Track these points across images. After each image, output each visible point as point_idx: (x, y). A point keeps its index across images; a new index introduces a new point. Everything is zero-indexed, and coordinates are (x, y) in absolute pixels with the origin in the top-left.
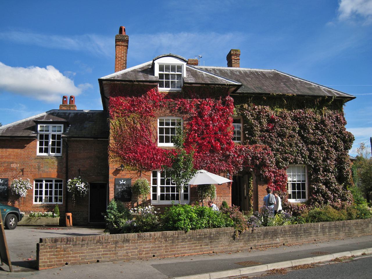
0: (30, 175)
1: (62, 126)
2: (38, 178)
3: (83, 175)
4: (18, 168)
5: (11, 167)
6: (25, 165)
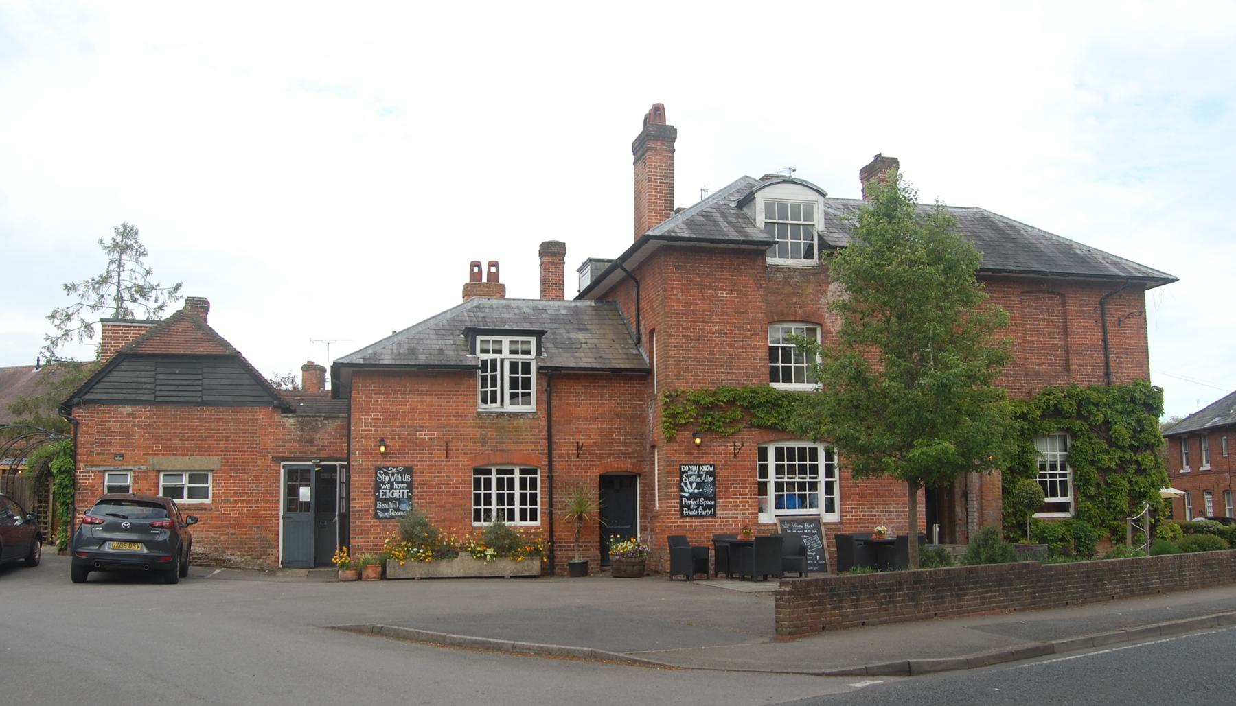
0: (462, 457)
1: (533, 340)
2: (479, 464)
3: (587, 458)
4: (433, 442)
5: (417, 439)
6: (450, 435)
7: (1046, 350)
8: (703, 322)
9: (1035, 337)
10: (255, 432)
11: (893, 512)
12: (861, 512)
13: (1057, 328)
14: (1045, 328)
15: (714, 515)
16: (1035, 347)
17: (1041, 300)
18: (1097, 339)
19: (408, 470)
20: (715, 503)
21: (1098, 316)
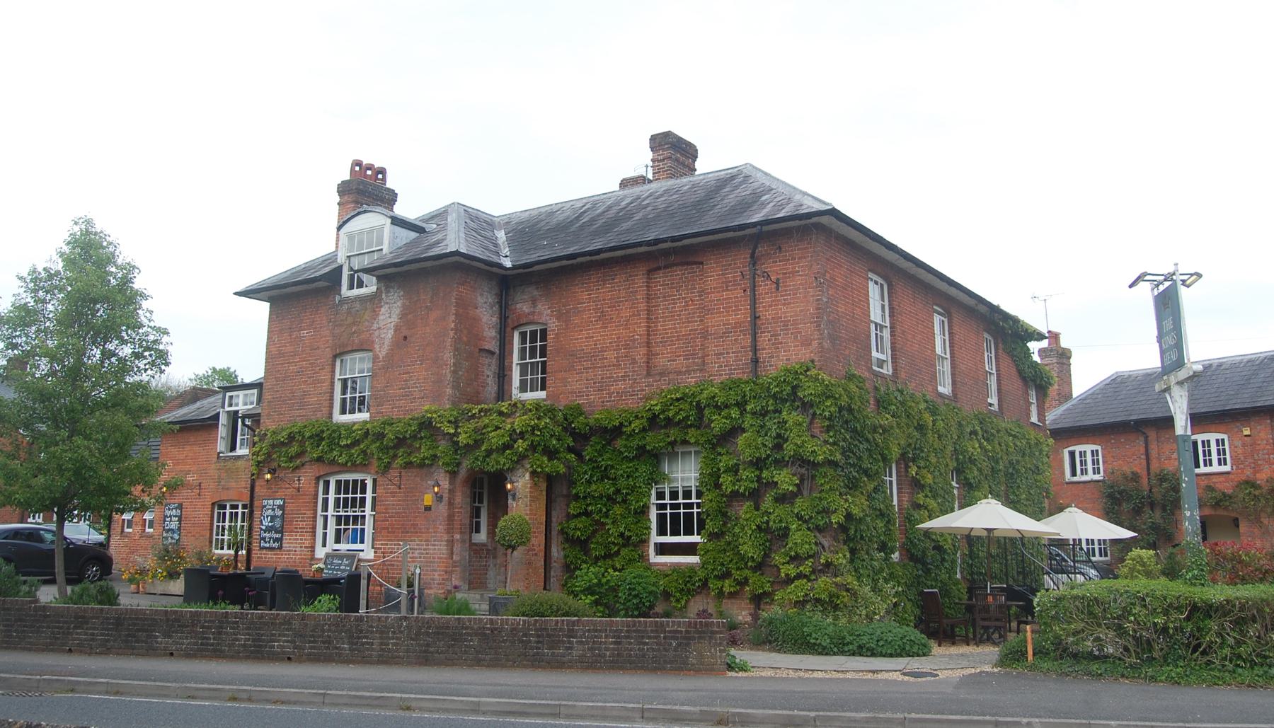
7: (681, 340)
8: (288, 363)
9: (668, 325)
10: (1089, 458)
11: (416, 549)
12: (389, 548)
13: (698, 309)
14: (682, 311)
15: (280, 548)
16: (668, 337)
17: (678, 275)
18: (743, 315)
19: (180, 507)
20: (282, 536)
21: (746, 283)
